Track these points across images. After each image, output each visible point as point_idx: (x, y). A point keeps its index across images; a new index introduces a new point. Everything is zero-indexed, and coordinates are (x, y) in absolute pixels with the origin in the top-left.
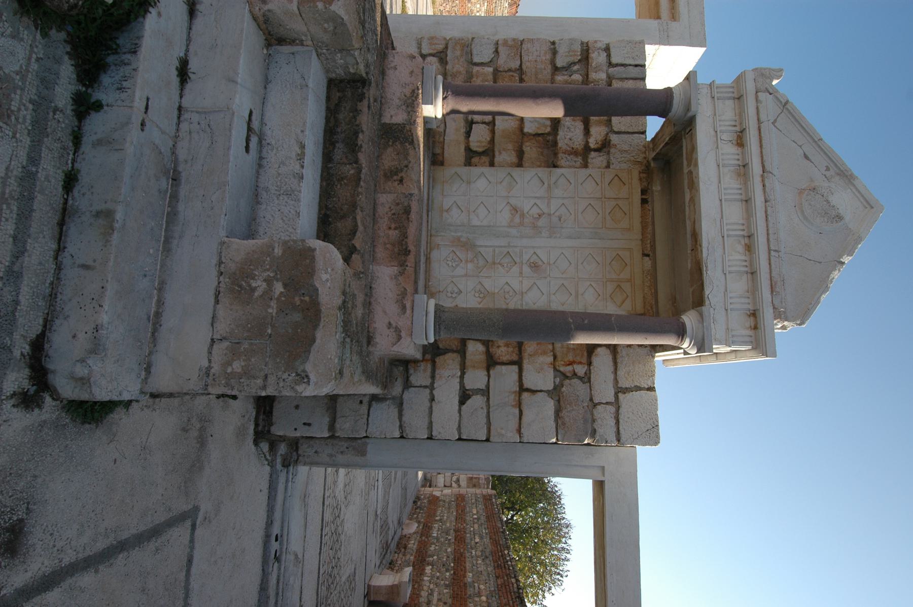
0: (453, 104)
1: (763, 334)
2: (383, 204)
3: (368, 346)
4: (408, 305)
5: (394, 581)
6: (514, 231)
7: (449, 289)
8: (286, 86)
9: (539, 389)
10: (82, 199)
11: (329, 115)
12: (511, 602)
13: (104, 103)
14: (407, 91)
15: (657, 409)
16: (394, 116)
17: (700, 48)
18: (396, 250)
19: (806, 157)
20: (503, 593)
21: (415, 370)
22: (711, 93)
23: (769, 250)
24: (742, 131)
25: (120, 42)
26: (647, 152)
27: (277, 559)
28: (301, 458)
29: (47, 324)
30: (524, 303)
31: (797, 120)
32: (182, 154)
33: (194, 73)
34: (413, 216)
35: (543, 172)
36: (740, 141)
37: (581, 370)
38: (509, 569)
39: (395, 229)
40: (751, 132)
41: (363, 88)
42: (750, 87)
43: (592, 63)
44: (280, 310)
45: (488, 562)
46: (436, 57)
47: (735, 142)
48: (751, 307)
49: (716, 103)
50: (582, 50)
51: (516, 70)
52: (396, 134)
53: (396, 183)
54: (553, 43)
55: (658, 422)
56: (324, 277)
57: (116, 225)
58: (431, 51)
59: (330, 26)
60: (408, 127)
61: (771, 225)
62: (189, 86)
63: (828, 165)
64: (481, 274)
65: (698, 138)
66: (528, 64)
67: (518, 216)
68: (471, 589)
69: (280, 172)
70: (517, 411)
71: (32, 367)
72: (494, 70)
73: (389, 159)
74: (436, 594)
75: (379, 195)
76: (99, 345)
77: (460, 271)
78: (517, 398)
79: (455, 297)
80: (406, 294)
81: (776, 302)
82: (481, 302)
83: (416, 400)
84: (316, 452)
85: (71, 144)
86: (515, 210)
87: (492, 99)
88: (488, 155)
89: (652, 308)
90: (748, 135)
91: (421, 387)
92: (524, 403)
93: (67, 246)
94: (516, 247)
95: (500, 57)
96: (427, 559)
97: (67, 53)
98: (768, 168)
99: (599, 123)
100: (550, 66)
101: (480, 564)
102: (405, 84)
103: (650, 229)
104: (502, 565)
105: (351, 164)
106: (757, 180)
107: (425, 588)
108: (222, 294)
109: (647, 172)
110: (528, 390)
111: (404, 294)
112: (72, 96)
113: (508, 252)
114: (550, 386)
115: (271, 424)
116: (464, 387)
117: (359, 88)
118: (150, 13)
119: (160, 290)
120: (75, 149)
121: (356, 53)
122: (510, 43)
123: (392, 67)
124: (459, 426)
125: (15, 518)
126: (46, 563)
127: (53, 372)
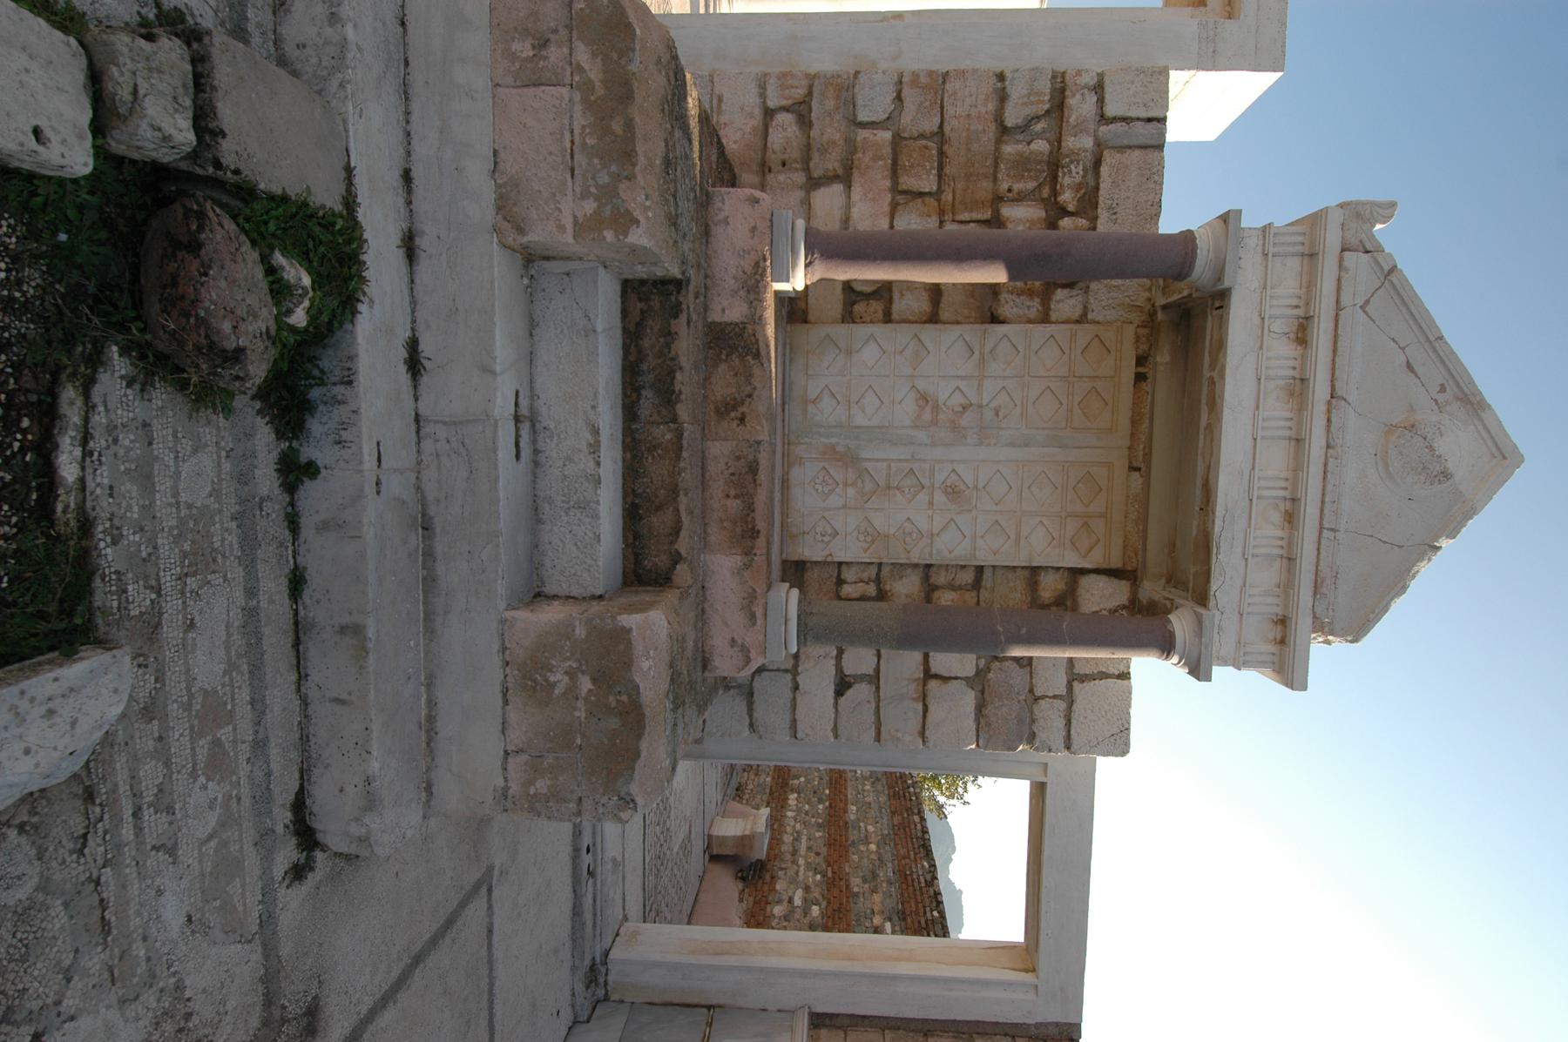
0: (821, 271)
1: (1291, 656)
2: (716, 457)
3: (703, 672)
4: (759, 614)
5: (745, 830)
6: (921, 435)
7: (819, 529)
8: (562, 332)
9: (953, 675)
10: (315, 608)
11: (628, 341)
12: (912, 853)
13: (319, 463)
14: (747, 264)
15: (1130, 706)
16: (730, 310)
17: (1273, 74)
18: (738, 530)
19: (1410, 367)
20: (900, 838)
22: (1264, 245)
23: (1321, 528)
25: (325, 363)
26: (1154, 289)
27: (591, 873)
29: (304, 774)
30: (934, 552)
31: (1404, 303)
32: (431, 492)
33: (429, 359)
34: (762, 476)
36: (1302, 335)
38: (911, 800)
39: (736, 497)
40: (1321, 325)
41: (678, 293)
42: (1332, 239)
43: (1069, 117)
44: (590, 714)
45: (879, 787)
46: (792, 112)
47: (1292, 336)
48: (1279, 610)
49: (1270, 264)
50: (1053, 90)
51: (934, 134)
52: (731, 342)
53: (735, 423)
54: (1001, 77)
55: (1129, 723)
56: (645, 665)
57: (370, 645)
58: (784, 103)
60: (750, 328)
61: (1329, 487)
62: (425, 380)
63: (1444, 382)
64: (869, 505)
65: (1230, 331)
66: (955, 123)
67: (928, 409)
68: (855, 832)
69: (566, 473)
70: (920, 707)
71: (298, 833)
72: (894, 137)
73: (723, 383)
74: (804, 839)
75: (710, 443)
76: (375, 801)
77: (835, 501)
78: (921, 689)
79: (829, 542)
80: (756, 597)
81: (1319, 610)
82: (868, 548)
85: (287, 532)
86: (924, 398)
89: (1136, 555)
90: (1315, 330)
91: (778, 670)
92: (930, 694)
93: (309, 673)
94: (924, 461)
95: (906, 110)
96: (791, 782)
97: (259, 412)
98: (1339, 392)
100: (993, 127)
101: (868, 791)
102: (744, 251)
103: (1145, 426)
104: (901, 792)
105: (667, 423)
106: (1320, 409)
107: (789, 829)
108: (510, 692)
110: (936, 677)
111: (751, 597)
112: (276, 467)
113: (912, 469)
114: (971, 672)
116: (842, 672)
117: (671, 294)
118: (360, 313)
119: (429, 686)
120: (293, 537)
122: (924, 80)
123: (720, 221)
124: (835, 725)
125: (309, 999)
126: (346, 1024)
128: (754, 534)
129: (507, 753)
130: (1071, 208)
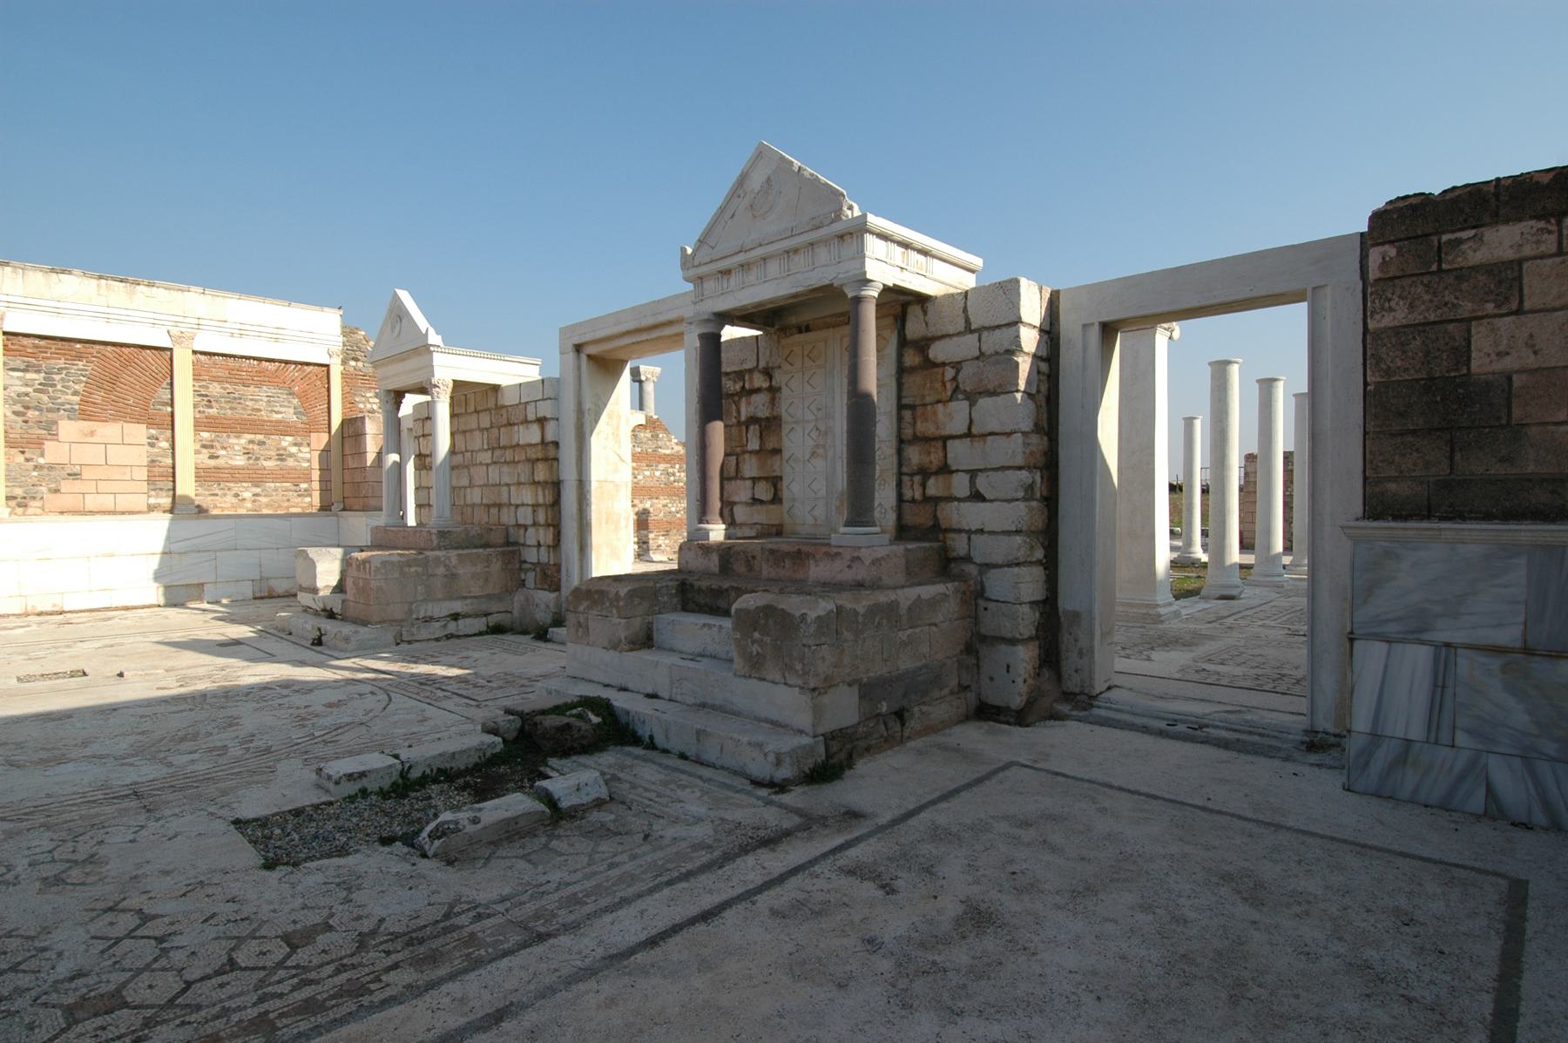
4: (835, 550)
16: (714, 563)
19: (733, 216)
21: (954, 551)
24: (721, 272)
28: (1086, 691)
32: (691, 700)
35: (785, 429)
36: (726, 272)
37: (950, 373)
44: (768, 634)
59: (637, 601)
62: (660, 694)
70: (990, 438)
73: (740, 568)
83: (985, 550)
84: (1076, 671)
87: (707, 483)
88: (775, 482)
91: (969, 545)
99: (751, 380)
109: (785, 331)
110: (969, 429)
111: (827, 554)
115: (1008, 708)
121: (658, 585)
127: (772, 777)
128: (799, 551)
129: (785, 684)
130: (741, 384)
